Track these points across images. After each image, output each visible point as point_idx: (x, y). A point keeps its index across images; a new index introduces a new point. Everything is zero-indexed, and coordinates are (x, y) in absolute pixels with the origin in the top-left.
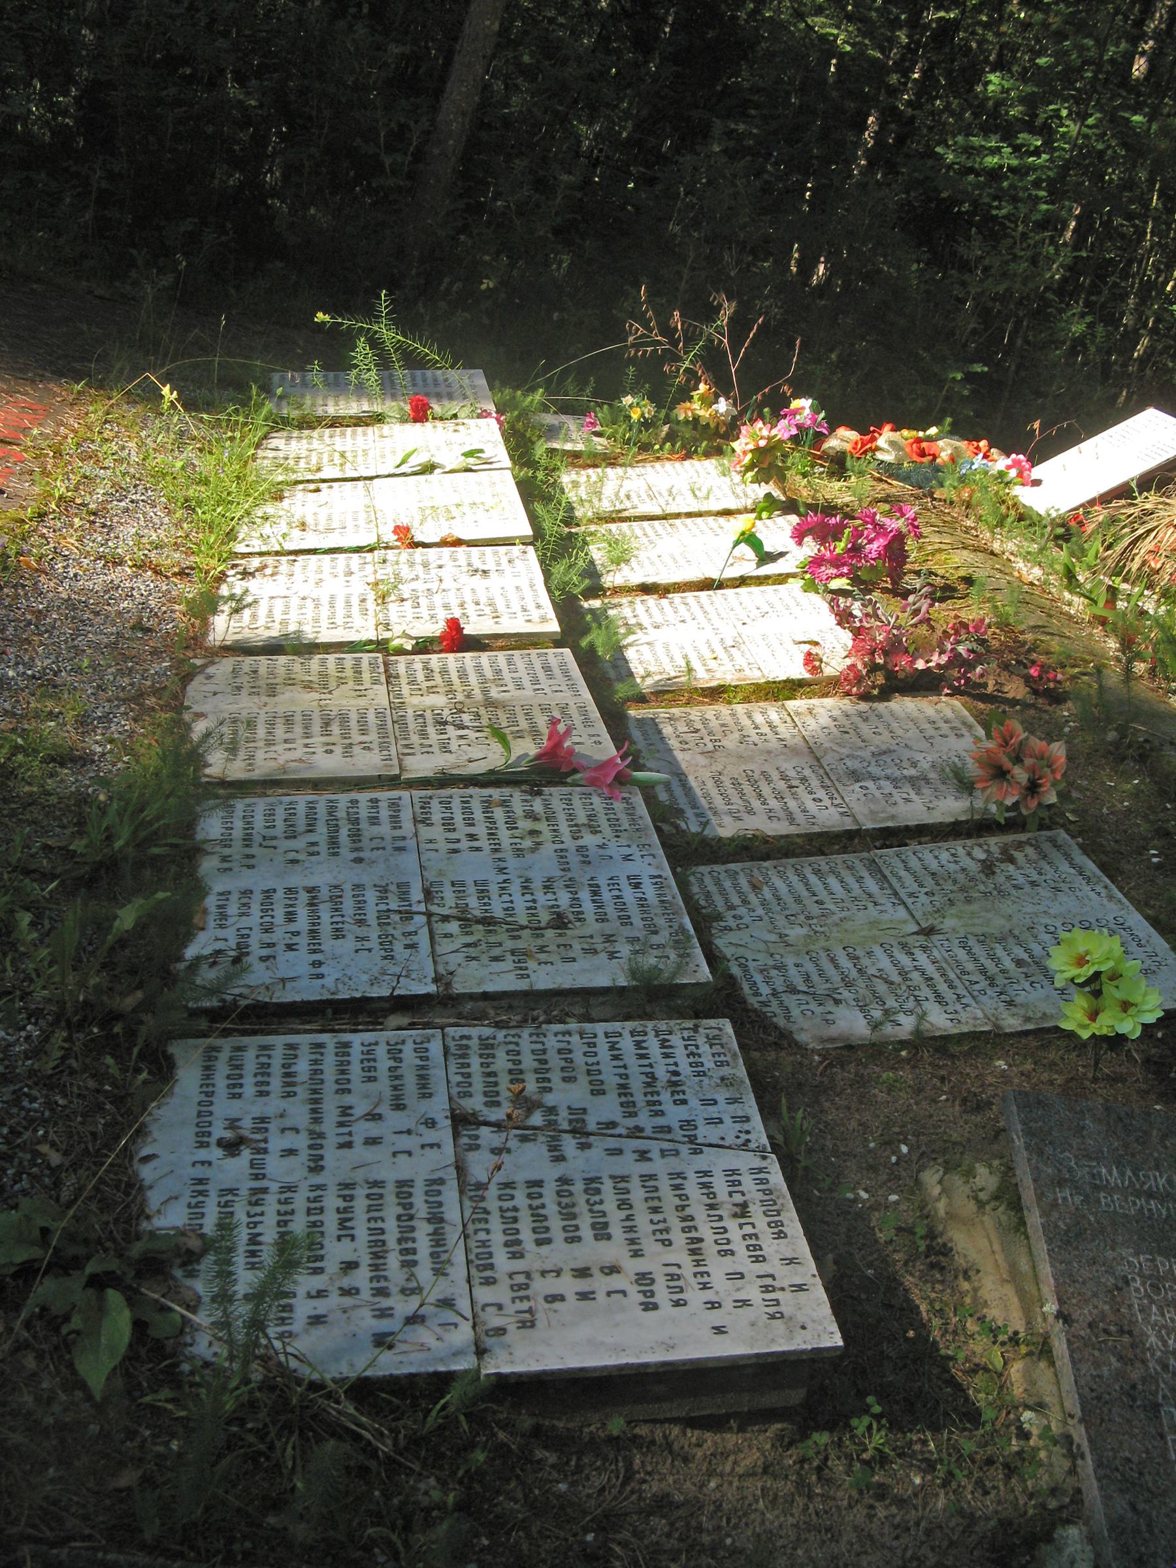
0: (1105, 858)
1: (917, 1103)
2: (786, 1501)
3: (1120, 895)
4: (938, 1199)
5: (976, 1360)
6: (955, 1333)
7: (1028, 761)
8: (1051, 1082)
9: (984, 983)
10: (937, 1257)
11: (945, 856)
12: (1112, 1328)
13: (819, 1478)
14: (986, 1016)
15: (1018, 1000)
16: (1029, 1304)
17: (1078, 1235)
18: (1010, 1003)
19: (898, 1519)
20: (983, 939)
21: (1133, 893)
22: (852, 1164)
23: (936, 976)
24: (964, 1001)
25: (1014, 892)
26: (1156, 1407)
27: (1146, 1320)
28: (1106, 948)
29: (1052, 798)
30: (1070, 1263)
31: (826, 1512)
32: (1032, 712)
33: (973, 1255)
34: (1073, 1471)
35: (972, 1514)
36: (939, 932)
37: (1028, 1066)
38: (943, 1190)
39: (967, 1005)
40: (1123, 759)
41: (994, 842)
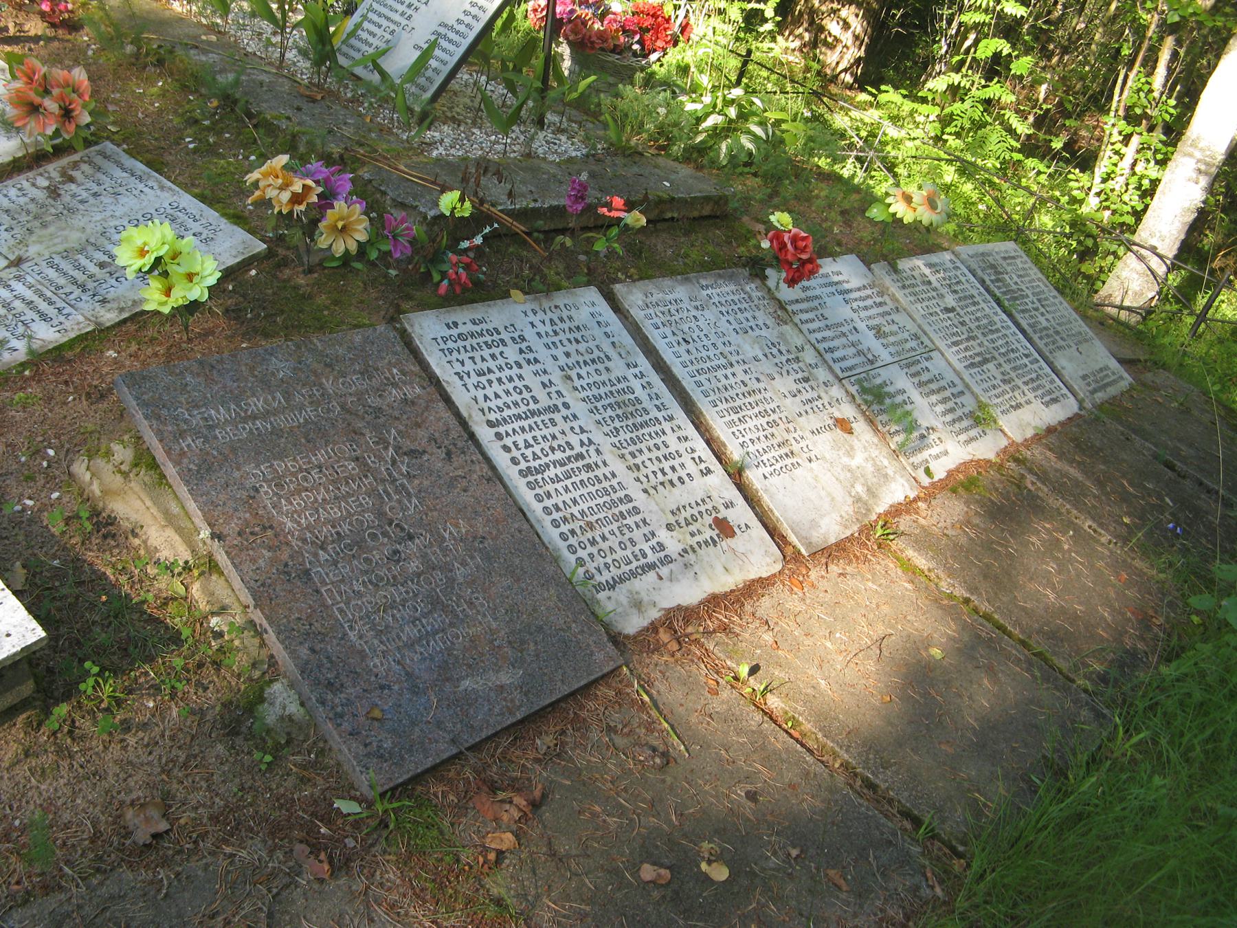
0: (149, 156)
1: (51, 411)
2: (53, 769)
3: (170, 184)
4: (91, 483)
5: (165, 595)
6: (141, 581)
7: (56, 92)
8: (156, 354)
9: (77, 292)
10: (106, 528)
11: (13, 193)
12: (257, 529)
13: (73, 739)
14: (87, 319)
15: (109, 297)
16: (188, 537)
17: (208, 470)
18: (104, 301)
19: (146, 739)
20: (66, 254)
21: (180, 178)
22: (11, 481)
23: (35, 298)
24: (64, 312)
25: (81, 207)
26: (307, 572)
27: (280, 512)
28: (158, 235)
29: (87, 119)
30: (208, 493)
31: (88, 762)
32: (56, 44)
33: (134, 517)
34: (263, 644)
35: (201, 709)
36: (27, 260)
37: (134, 347)
38: (93, 475)
39: (69, 315)
40: (145, 68)
41: (53, 169)
